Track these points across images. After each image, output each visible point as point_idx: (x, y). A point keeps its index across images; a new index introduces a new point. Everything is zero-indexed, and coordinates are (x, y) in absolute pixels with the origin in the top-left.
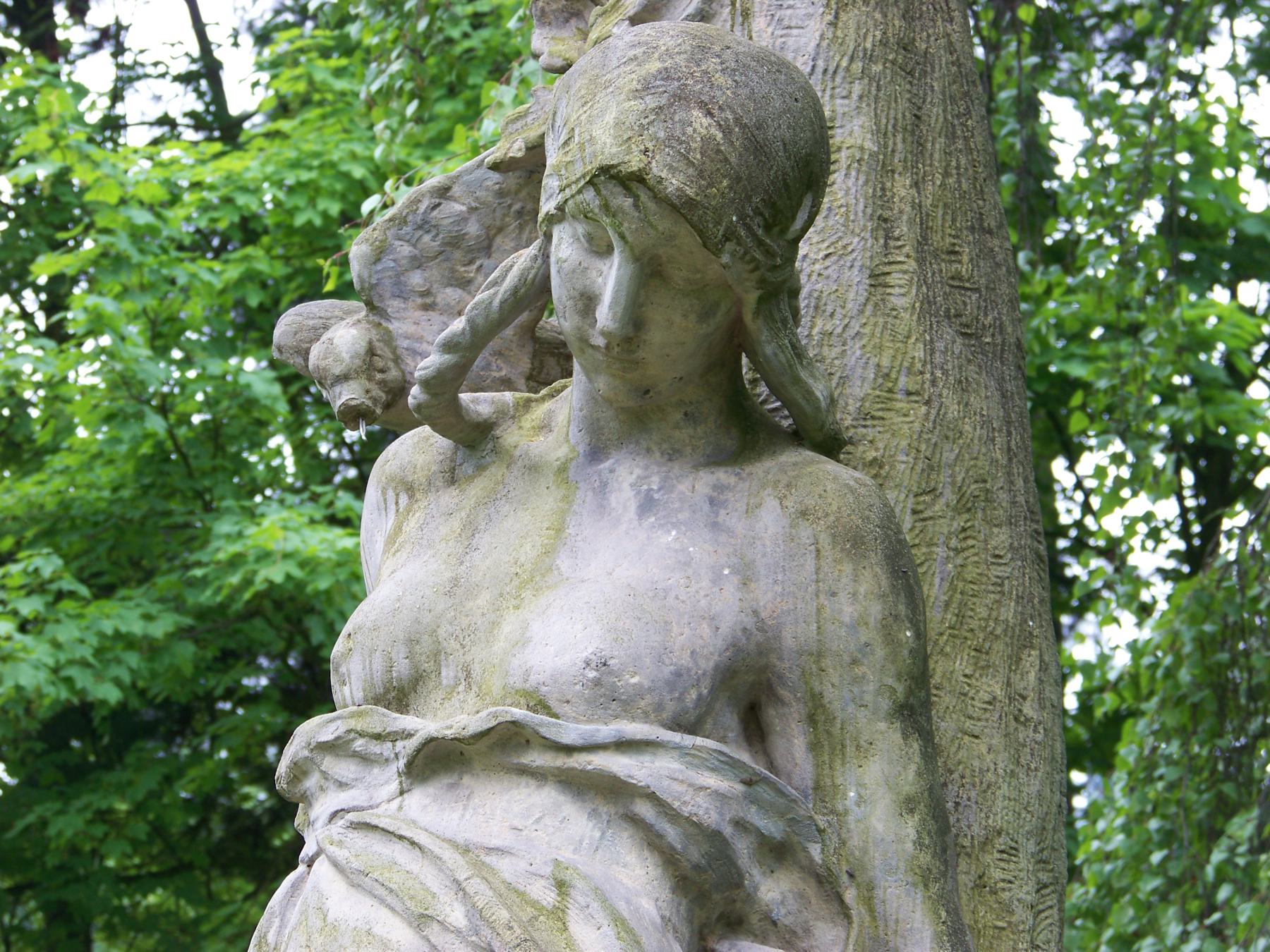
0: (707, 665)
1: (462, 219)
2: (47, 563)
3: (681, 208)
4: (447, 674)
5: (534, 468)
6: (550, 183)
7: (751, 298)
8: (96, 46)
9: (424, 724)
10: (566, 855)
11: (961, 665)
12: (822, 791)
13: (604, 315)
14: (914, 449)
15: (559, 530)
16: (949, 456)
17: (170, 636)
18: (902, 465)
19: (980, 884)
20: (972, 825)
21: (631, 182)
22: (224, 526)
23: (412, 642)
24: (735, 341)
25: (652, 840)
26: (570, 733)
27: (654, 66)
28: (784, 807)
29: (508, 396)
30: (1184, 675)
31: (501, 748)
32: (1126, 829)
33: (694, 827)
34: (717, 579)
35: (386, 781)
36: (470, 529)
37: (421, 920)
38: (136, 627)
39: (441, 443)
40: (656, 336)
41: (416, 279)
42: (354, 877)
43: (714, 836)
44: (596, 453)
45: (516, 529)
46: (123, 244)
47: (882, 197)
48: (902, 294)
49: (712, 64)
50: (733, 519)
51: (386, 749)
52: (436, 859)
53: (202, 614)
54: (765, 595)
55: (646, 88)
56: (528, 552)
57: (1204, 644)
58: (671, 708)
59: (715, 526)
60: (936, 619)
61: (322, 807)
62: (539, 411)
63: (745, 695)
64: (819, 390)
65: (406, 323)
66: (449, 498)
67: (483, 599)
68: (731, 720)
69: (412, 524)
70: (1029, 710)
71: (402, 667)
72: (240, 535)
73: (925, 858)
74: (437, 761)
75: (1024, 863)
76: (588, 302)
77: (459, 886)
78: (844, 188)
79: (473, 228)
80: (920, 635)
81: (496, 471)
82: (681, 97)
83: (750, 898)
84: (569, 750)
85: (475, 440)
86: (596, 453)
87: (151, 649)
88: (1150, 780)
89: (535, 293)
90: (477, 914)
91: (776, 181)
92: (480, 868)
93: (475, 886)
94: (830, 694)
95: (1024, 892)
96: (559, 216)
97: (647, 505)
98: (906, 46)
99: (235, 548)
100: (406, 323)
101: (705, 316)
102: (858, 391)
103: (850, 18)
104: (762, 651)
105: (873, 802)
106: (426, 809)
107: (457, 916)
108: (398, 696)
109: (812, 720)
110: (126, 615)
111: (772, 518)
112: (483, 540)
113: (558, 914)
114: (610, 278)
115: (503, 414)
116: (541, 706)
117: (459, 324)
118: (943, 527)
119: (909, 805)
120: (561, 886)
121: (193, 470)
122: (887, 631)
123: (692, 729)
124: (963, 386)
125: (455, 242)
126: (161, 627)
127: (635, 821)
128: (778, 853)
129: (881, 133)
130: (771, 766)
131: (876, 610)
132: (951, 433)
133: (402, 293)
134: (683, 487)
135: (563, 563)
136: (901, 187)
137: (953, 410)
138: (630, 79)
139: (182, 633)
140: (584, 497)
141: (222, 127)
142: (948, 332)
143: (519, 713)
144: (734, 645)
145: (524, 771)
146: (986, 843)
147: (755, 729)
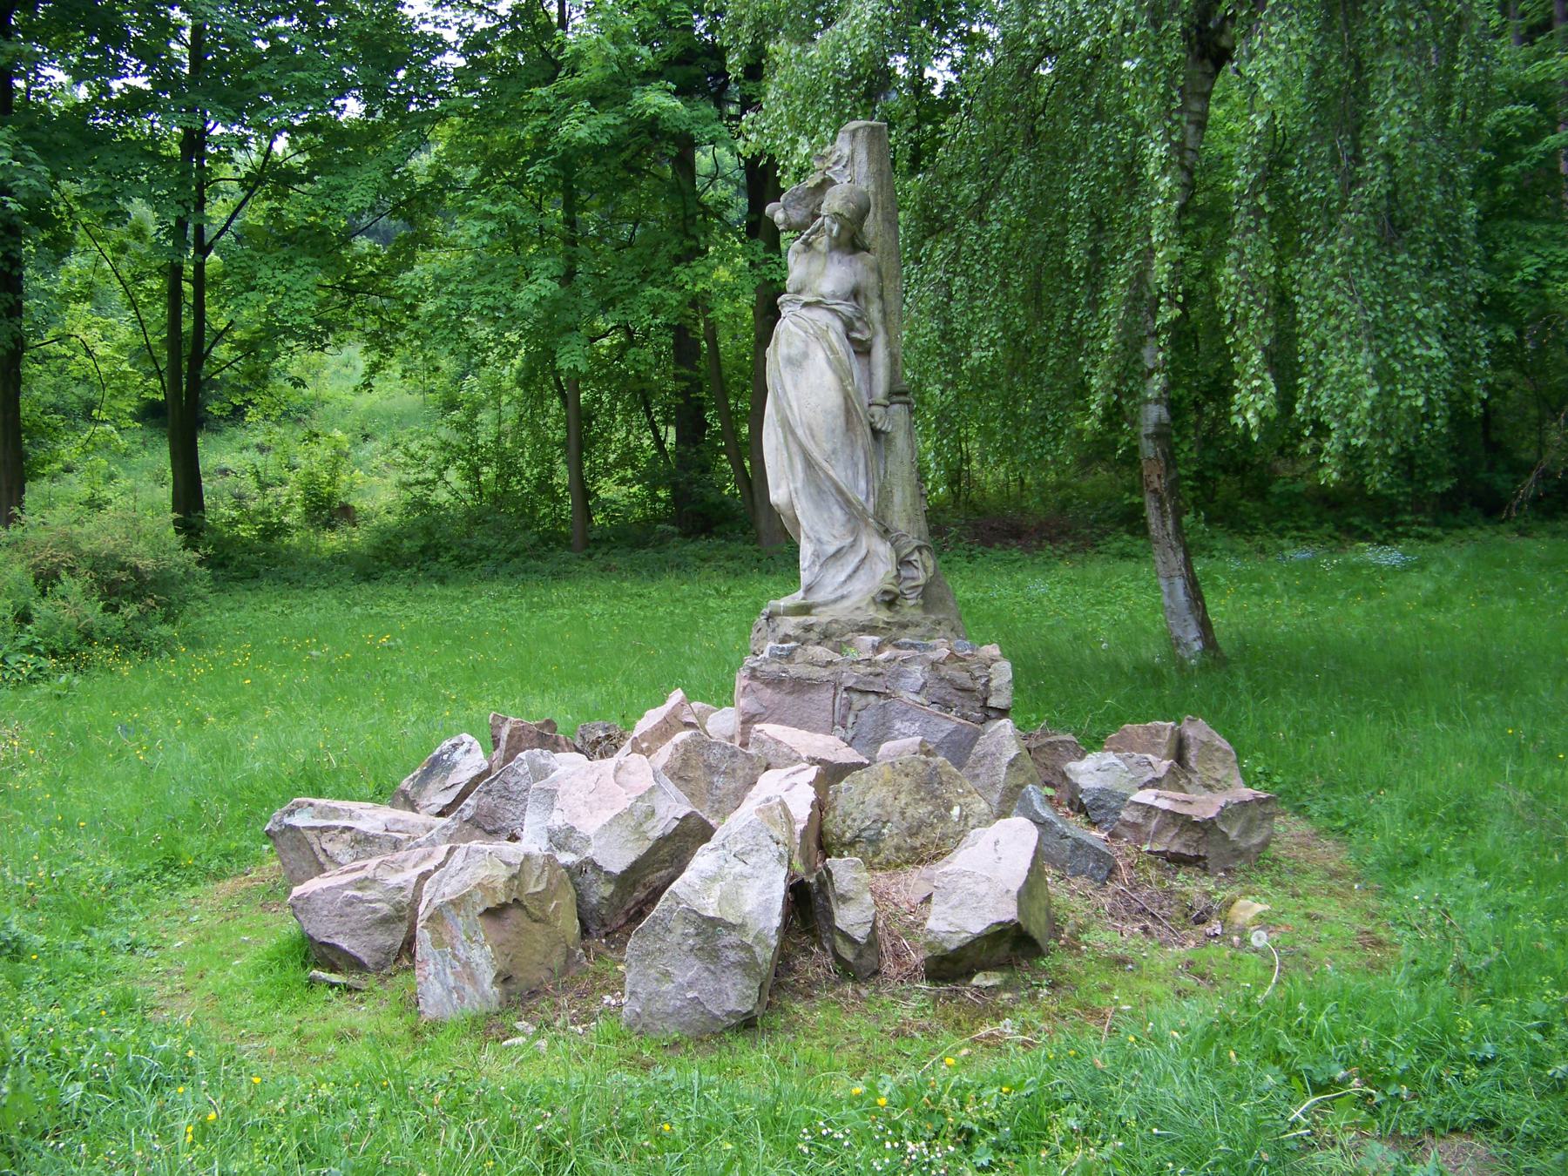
9: (805, 298)
44: (831, 250)
45: (817, 265)
63: (855, 294)
74: (806, 305)
86: (831, 250)
91: (862, 213)
105: (875, 311)
108: (798, 292)
111: (859, 265)
126: (618, 122)
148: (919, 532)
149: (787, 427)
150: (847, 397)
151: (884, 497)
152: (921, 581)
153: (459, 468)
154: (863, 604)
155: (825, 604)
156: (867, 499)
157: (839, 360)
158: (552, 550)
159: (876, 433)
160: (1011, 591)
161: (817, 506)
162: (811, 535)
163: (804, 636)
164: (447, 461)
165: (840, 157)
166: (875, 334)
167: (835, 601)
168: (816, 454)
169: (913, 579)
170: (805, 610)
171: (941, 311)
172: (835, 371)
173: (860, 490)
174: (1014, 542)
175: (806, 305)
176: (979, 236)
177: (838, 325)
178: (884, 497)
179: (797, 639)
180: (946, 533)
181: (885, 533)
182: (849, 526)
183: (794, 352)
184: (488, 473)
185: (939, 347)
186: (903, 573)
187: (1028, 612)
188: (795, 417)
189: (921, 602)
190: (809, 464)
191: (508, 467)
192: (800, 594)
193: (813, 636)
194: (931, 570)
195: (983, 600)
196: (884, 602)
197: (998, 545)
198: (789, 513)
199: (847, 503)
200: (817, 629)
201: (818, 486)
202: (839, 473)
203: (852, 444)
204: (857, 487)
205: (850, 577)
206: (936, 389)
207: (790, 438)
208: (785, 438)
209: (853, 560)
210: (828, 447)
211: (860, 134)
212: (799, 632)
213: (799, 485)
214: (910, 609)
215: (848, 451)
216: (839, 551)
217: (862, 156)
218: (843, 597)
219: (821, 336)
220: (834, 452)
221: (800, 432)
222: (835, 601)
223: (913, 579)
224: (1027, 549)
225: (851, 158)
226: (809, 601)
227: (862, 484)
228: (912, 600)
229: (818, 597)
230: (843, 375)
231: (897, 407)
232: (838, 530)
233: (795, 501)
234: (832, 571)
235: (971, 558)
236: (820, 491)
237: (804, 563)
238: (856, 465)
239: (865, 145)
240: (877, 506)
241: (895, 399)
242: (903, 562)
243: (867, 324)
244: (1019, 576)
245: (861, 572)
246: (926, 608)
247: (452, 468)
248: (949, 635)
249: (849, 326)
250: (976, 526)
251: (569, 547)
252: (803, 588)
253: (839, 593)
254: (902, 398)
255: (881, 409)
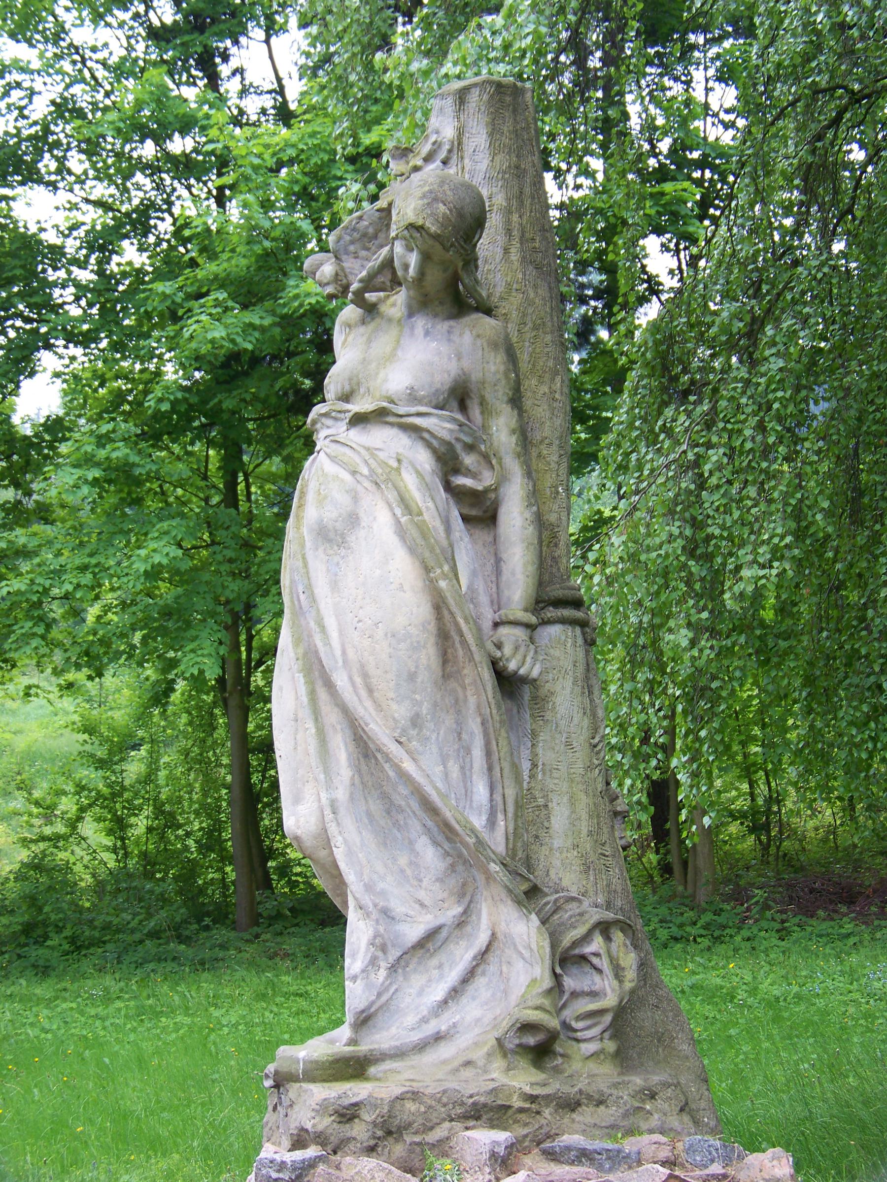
0: (447, 387)
1: (367, 227)
2: (222, 295)
3: (436, 237)
4: (362, 390)
5: (390, 320)
6: (393, 227)
7: (461, 264)
8: (234, 74)
9: (355, 408)
10: (400, 450)
11: (534, 382)
12: (485, 428)
13: (412, 271)
14: (518, 309)
15: (398, 342)
16: (530, 311)
17: (271, 325)
18: (514, 314)
19: (539, 455)
20: (537, 436)
21: (420, 228)
22: (291, 282)
23: (350, 379)
24: (455, 279)
25: (429, 445)
26: (402, 410)
27: (427, 188)
28: (472, 434)
29: (382, 294)
30: (649, 355)
31: (379, 416)
32: (627, 413)
33: (443, 441)
34: (450, 358)
35: (343, 426)
36: (369, 341)
37: (354, 473)
38: (257, 322)
39: (360, 311)
40: (429, 278)
41: (352, 248)
42: (332, 458)
43: (449, 444)
44: (410, 315)
45: (384, 342)
46: (249, 171)
47: (508, 222)
48: (515, 256)
49: (446, 187)
50: (455, 337)
51: (342, 416)
52: (359, 453)
53: (283, 317)
54: (466, 364)
55: (424, 196)
56: (388, 349)
57: (656, 343)
58: (434, 402)
59: (449, 340)
60: (524, 365)
61: (322, 434)
62: (392, 299)
63: (459, 396)
64: (484, 294)
65: (349, 263)
66: (362, 329)
67: (374, 365)
68: (455, 404)
69: (350, 339)
70: (557, 396)
71: (347, 388)
72: (297, 286)
73: (519, 449)
74: (358, 420)
75: (555, 448)
76: (406, 267)
77: (366, 462)
78: (494, 221)
79: (371, 230)
80: (517, 376)
81: (378, 320)
82: (436, 200)
83: (461, 463)
84: (401, 416)
85: (371, 310)
86: (410, 315)
87: (262, 329)
88: (636, 394)
89: (389, 263)
90: (372, 470)
91: (468, 224)
92: (373, 455)
93: (371, 461)
94: (487, 396)
95: (555, 458)
96: (396, 238)
97: (427, 333)
98: (517, 167)
99: (296, 291)
100: (349, 263)
101: (445, 271)
102: (500, 289)
103: (498, 159)
104: (465, 382)
105: (502, 431)
106: (355, 436)
107: (366, 471)
108: (346, 398)
109: (481, 404)
110: (254, 317)
112: (373, 345)
113: (398, 470)
114: (413, 259)
115: (381, 301)
116: (392, 402)
117: (364, 273)
118: (528, 335)
119: (513, 432)
120: (399, 461)
121: (279, 258)
122: (506, 374)
123: (442, 409)
124: (535, 287)
125: (365, 235)
126: (267, 322)
127: (423, 439)
128: (470, 448)
129: (508, 199)
130: (469, 419)
131: (502, 368)
132: (531, 303)
133: (347, 253)
134: (439, 327)
135: (400, 353)
136: (515, 218)
137: (532, 295)
138: (419, 193)
139: (274, 324)
140: (406, 330)
141: (284, 115)
142: (531, 268)
143: (385, 404)
144: (455, 381)
145: (387, 423)
146: (541, 442)
147: (463, 407)
148: (609, 889)
149: (316, 672)
150: (439, 606)
151: (527, 816)
152: (610, 1000)
153: (99, 820)
154: (478, 1056)
155: (399, 1054)
156: (492, 823)
157: (424, 531)
158: (207, 928)
159: (508, 683)
160: (841, 982)
161: (385, 841)
162: (367, 900)
163: (337, 1131)
164: (82, 810)
165: (437, 145)
166: (503, 479)
167: (421, 1047)
168: (380, 731)
169: (593, 994)
170: (353, 1067)
171: (686, 508)
172: (412, 550)
173: (475, 806)
174: (844, 909)
175: (358, 420)
176: (747, 383)
177: (424, 459)
178: (527, 816)
179: (320, 1139)
180: (749, 898)
181: (530, 895)
182: (453, 882)
183: (330, 514)
184: (140, 824)
185: (684, 566)
186: (570, 983)
187: (867, 1015)
188: (331, 653)
189: (611, 1046)
190: (364, 748)
191: (166, 820)
192: (344, 1032)
193: (359, 1131)
194: (631, 975)
195: (798, 997)
196: (523, 1049)
197: (821, 913)
198: (322, 854)
199: (446, 832)
200: (368, 1116)
201: (385, 797)
202: (427, 767)
203: (458, 706)
204: (468, 793)
205: (455, 993)
206: (683, 637)
207: (323, 695)
208: (312, 695)
209: (462, 955)
210: (401, 711)
211: (474, 97)
212: (325, 1123)
213: (341, 794)
214: (587, 1062)
215: (449, 721)
216: (432, 935)
217: (478, 138)
218: (438, 1038)
219: (384, 479)
220: (416, 721)
221: (341, 680)
222: (421, 1047)
223: (593, 994)
224: (863, 918)
225: (458, 145)
226: (363, 1048)
227: (481, 791)
228: (591, 1042)
229: (380, 1039)
230: (432, 560)
231: (555, 630)
232: (430, 890)
233: (333, 829)
234: (417, 980)
235: (783, 933)
236: (391, 808)
237: (355, 959)
238: (468, 751)
239: (485, 119)
240: (514, 836)
241: (551, 613)
242: (566, 960)
243: (486, 457)
244: (854, 959)
245: (480, 982)
246: (623, 1058)
247: (88, 817)
248: (674, 1122)
249: (448, 463)
250: (790, 886)
251: (234, 926)
252: (349, 1018)
253: (430, 1029)
254: (567, 612)
255: (520, 633)
